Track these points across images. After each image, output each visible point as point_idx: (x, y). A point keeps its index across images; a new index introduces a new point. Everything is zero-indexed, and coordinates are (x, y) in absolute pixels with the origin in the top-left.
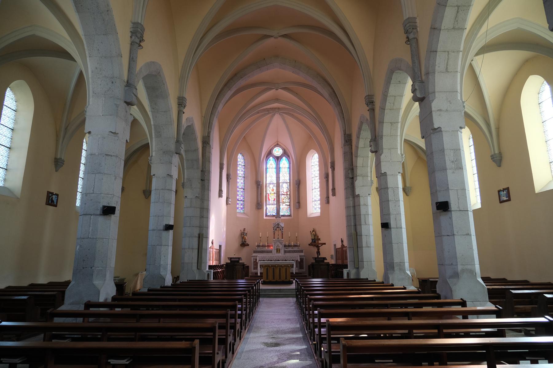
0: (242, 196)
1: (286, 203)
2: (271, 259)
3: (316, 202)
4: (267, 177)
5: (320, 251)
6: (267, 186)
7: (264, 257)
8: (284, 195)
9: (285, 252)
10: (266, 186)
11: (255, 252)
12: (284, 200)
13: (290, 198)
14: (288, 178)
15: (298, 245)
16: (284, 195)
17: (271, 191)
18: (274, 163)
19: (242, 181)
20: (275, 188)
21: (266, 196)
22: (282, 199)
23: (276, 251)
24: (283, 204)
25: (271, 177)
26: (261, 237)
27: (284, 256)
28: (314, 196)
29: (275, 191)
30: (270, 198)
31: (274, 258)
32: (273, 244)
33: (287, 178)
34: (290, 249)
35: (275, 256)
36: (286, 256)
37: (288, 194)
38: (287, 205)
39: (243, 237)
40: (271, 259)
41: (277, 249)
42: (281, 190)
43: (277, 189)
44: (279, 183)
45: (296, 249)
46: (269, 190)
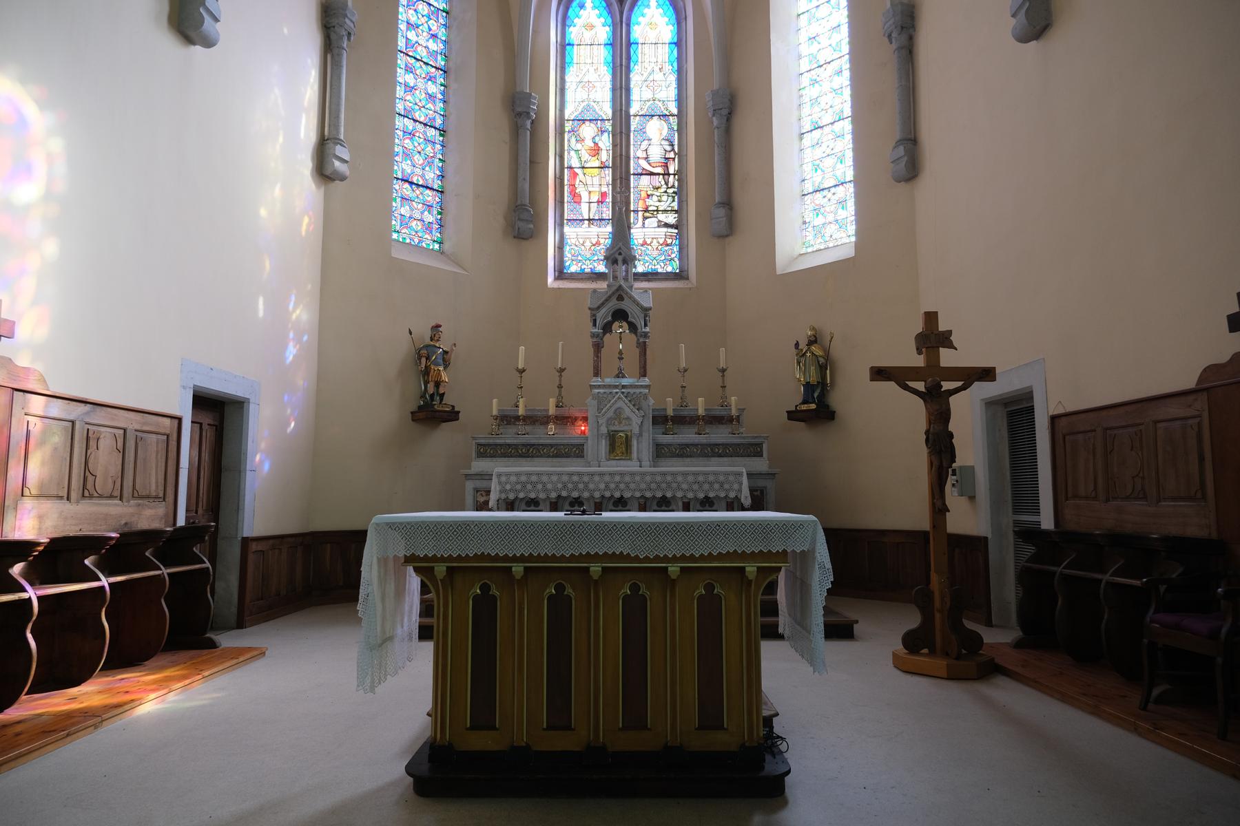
0: (429, 161)
1: (662, 217)
2: (575, 494)
3: (825, 192)
4: (568, 85)
5: (951, 428)
6: (567, 129)
7: (534, 478)
8: (652, 174)
9: (660, 452)
10: (560, 132)
11: (487, 451)
12: (649, 202)
13: (680, 193)
14: (672, 92)
15: (734, 412)
16: (652, 174)
17: (585, 156)
18: (602, 20)
19: (433, 88)
20: (606, 142)
21: (560, 180)
22: (643, 195)
23: (604, 445)
24: (645, 218)
25: (587, 85)
26: (522, 371)
27: (653, 474)
28: (808, 168)
29: (606, 156)
30: (580, 190)
31: (591, 486)
32: (592, 404)
33: (667, 93)
34: (688, 436)
35: (602, 474)
36: (664, 474)
37: (671, 171)
38: (667, 225)
39: (426, 372)
40: (576, 488)
41: (612, 438)
42: (636, 152)
43: (614, 145)
44: (628, 116)
45: (720, 435)
46: (577, 151)
